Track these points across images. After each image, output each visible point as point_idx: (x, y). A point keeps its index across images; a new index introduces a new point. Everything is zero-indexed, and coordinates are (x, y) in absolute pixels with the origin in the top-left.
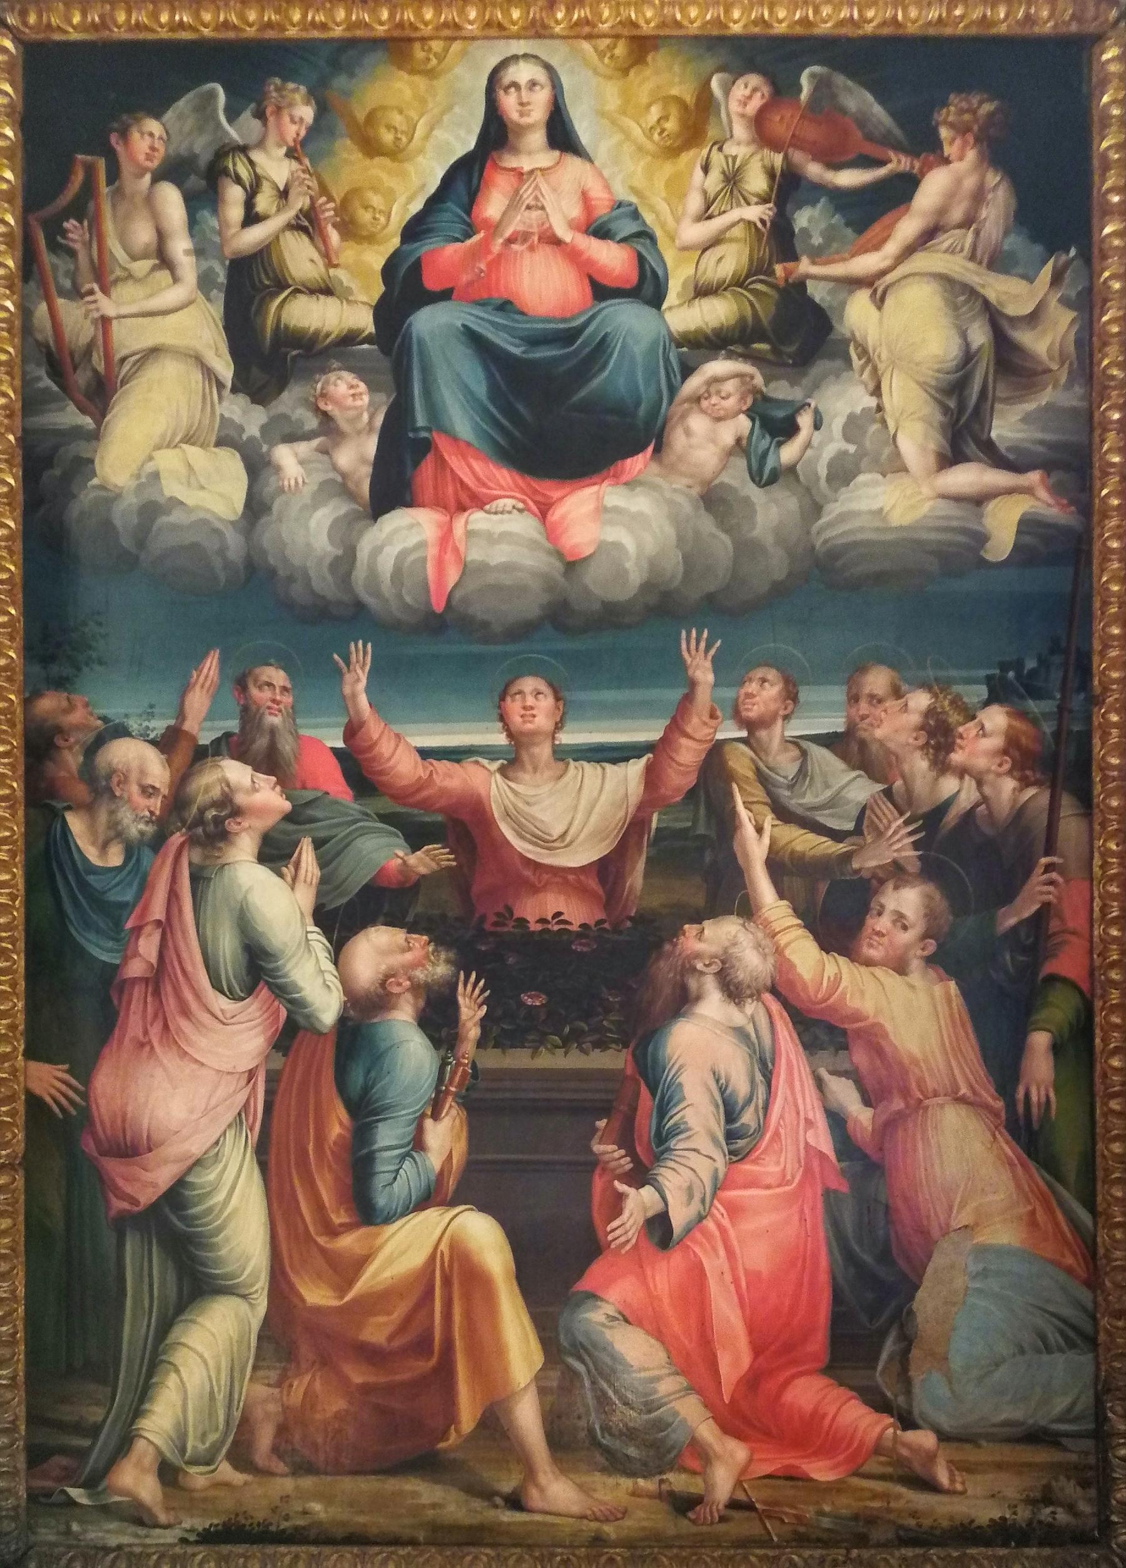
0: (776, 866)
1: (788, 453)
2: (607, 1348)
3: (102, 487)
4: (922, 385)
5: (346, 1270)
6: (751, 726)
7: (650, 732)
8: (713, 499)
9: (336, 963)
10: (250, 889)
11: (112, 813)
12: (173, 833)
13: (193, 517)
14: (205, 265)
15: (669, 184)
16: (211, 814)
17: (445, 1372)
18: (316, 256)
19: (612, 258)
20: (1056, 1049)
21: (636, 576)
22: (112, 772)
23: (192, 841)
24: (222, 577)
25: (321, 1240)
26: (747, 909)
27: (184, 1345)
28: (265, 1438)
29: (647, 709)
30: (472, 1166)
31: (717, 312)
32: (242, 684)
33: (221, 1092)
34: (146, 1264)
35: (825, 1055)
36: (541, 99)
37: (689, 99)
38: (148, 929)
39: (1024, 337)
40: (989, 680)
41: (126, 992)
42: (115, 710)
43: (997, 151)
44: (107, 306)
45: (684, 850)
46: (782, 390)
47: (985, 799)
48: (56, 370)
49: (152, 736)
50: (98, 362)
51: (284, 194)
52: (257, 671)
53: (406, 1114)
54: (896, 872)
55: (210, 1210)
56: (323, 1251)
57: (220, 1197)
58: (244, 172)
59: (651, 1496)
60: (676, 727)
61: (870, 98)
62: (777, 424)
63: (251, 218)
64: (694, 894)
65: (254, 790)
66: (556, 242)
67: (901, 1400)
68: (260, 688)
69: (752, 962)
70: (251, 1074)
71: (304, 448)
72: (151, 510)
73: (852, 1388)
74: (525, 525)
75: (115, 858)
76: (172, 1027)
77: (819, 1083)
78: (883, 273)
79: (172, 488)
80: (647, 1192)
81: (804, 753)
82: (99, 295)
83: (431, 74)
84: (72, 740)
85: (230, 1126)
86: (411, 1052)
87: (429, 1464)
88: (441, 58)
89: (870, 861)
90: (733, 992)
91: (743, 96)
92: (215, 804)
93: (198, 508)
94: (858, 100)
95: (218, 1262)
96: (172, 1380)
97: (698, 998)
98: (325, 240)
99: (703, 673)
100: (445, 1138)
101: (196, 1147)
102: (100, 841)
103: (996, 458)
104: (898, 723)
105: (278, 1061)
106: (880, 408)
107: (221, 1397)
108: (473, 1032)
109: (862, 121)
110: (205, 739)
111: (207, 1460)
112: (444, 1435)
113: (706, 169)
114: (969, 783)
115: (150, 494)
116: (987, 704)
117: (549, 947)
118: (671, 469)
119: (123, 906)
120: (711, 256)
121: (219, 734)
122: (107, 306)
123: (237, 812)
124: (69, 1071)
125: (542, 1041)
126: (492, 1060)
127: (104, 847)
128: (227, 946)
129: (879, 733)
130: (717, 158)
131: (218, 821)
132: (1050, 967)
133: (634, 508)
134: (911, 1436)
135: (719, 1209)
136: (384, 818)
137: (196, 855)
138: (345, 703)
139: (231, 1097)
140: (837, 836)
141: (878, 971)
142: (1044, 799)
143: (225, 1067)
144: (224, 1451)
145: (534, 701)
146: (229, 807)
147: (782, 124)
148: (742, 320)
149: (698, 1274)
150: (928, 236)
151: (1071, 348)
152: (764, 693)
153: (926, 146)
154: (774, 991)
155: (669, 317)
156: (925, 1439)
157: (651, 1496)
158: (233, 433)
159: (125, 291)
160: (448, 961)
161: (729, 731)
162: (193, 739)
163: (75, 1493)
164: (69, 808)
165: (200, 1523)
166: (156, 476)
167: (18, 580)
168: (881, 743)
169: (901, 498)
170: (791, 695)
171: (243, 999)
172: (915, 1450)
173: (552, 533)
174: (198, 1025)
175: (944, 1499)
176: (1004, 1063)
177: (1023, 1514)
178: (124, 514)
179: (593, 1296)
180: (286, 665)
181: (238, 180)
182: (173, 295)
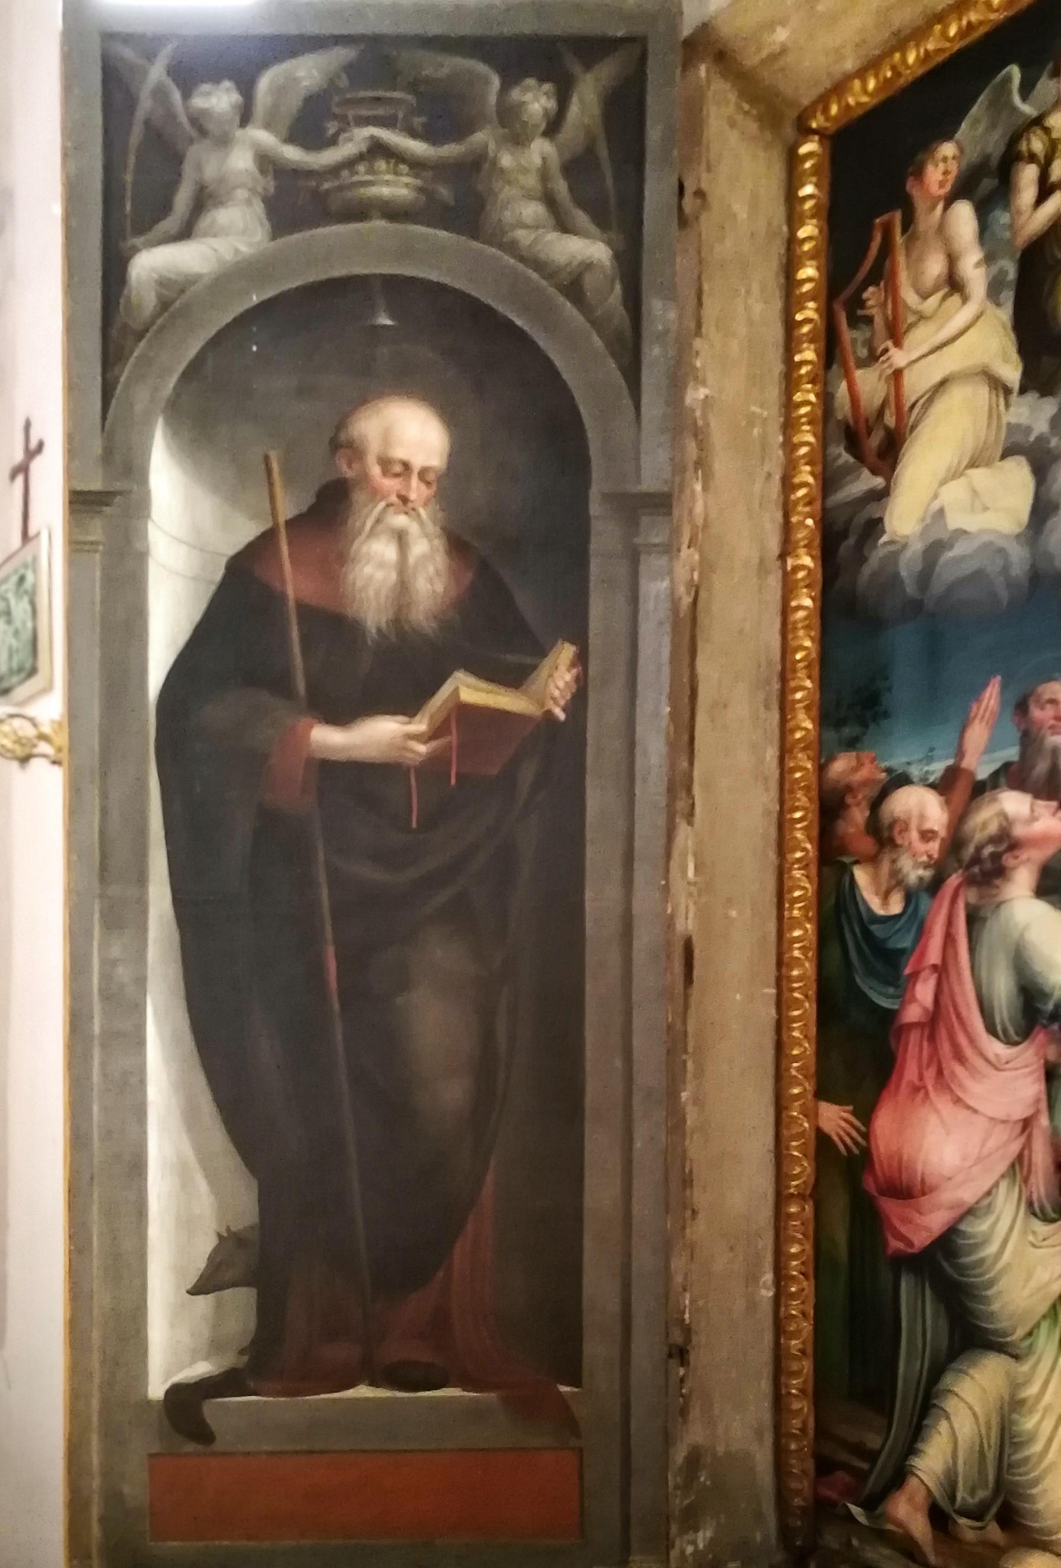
10: (1027, 927)
11: (894, 861)
12: (950, 875)
13: (976, 544)
14: (995, 269)
22: (894, 822)
23: (970, 881)
24: (1004, 595)
27: (957, 1395)
32: (1022, 707)
33: (992, 1143)
34: (920, 1302)
41: (903, 1037)
42: (897, 762)
44: (899, 358)
49: (932, 779)
50: (890, 420)
52: (1041, 689)
55: (982, 1261)
57: (992, 1249)
65: (1033, 818)
68: (1042, 708)
70: (1027, 1124)
72: (934, 550)
75: (896, 906)
76: (946, 1072)
79: (955, 521)
82: (893, 351)
84: (860, 797)
85: (1003, 1176)
92: (993, 840)
93: (982, 531)
95: (991, 1316)
96: (943, 1426)
101: (968, 1195)
102: (884, 888)
107: (991, 1455)
110: (983, 773)
111: (977, 1514)
115: (935, 535)
119: (902, 952)
121: (996, 766)
124: (854, 1113)
127: (886, 897)
128: (1003, 988)
131: (996, 857)
137: (971, 895)
143: (1000, 1114)
144: (994, 1510)
146: (1007, 842)
158: (1019, 438)
162: (971, 774)
163: (855, 1510)
164: (857, 862)
167: (814, 655)
171: (1016, 1044)
174: (973, 1072)
178: (908, 567)
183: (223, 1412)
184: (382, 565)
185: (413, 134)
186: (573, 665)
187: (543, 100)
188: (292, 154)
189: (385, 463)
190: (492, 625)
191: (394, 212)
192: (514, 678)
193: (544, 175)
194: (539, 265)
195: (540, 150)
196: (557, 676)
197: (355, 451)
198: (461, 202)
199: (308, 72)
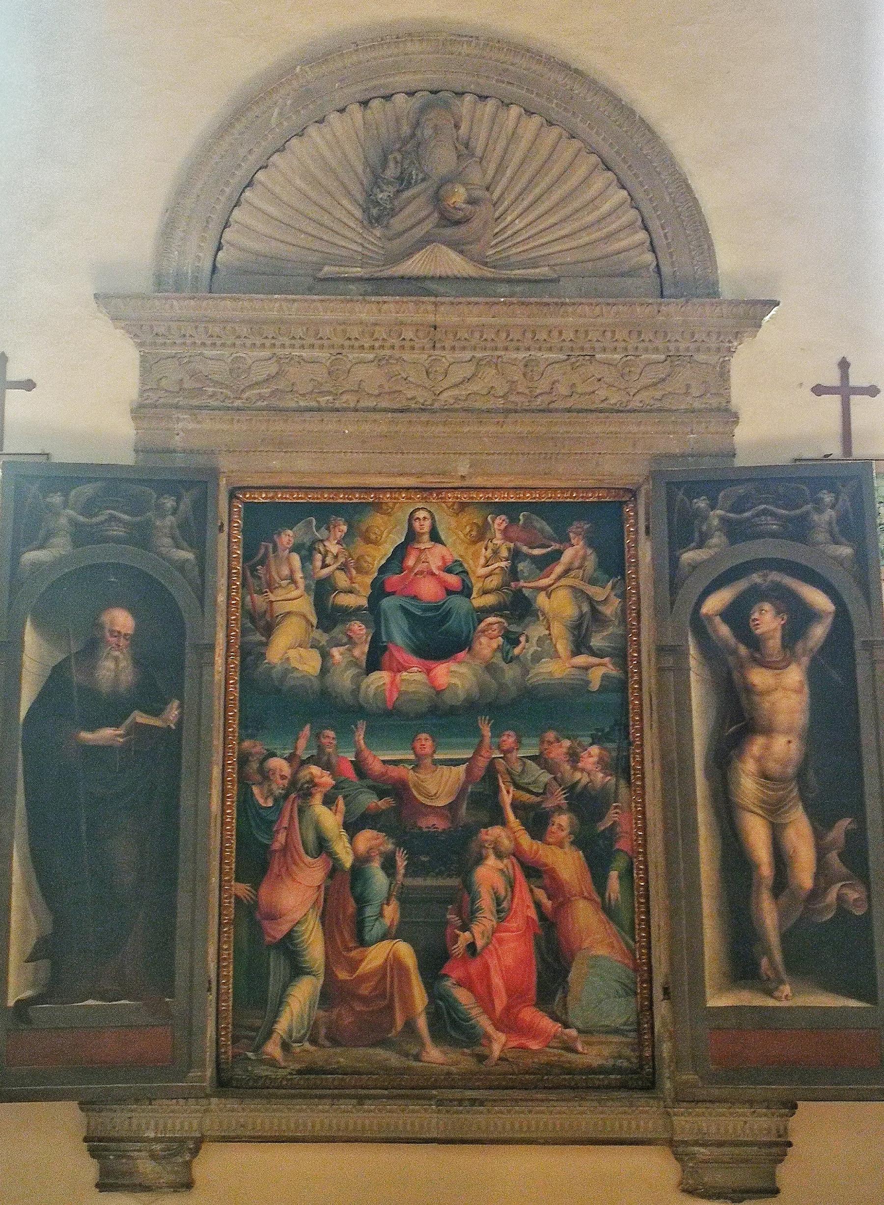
0: (515, 806)
1: (517, 651)
2: (450, 996)
3: (269, 663)
4: (566, 626)
5: (353, 965)
6: (505, 752)
7: (467, 754)
8: (490, 668)
9: (351, 844)
11: (269, 785)
15: (473, 554)
16: (306, 786)
17: (390, 1007)
18: (347, 579)
19: (453, 580)
20: (620, 877)
21: (462, 695)
23: (299, 796)
25: (344, 953)
26: (504, 823)
28: (323, 1031)
29: (465, 746)
30: (402, 923)
31: (490, 600)
32: (318, 736)
33: (307, 895)
35: (533, 880)
36: (427, 524)
37: (480, 524)
38: (282, 831)
39: (601, 608)
40: (592, 736)
43: (590, 543)
45: (483, 797)
46: (514, 628)
47: (591, 781)
48: (253, 620)
51: (336, 557)
53: (376, 903)
54: (559, 809)
55: (303, 941)
56: (344, 956)
58: (322, 549)
59: (469, 1055)
60: (477, 752)
61: (544, 523)
62: (512, 640)
63: (324, 566)
64: (484, 816)
66: (433, 574)
67: (564, 1017)
69: (506, 844)
71: (342, 649)
73: (546, 1012)
74: (421, 677)
77: (531, 891)
78: (550, 585)
79: (294, 664)
80: (467, 934)
81: (524, 763)
83: (389, 515)
86: (379, 879)
87: (383, 1043)
88: (392, 509)
89: (549, 804)
90: (499, 856)
91: (499, 523)
92: (308, 782)
94: (540, 524)
97: (486, 858)
98: (351, 574)
99: (487, 731)
100: (391, 912)
101: (298, 916)
103: (594, 654)
104: (559, 750)
105: (330, 882)
106: (550, 634)
108: (402, 871)
109: (542, 531)
110: (305, 757)
111: (300, 1041)
112: (389, 1031)
113: (486, 549)
114: (585, 774)
115: (286, 666)
116: (591, 744)
117: (431, 837)
118: (474, 657)
119: (272, 822)
120: (490, 579)
122: (272, 597)
123: (316, 785)
125: (427, 874)
126: (409, 882)
128: (311, 837)
129: (552, 755)
130: (490, 544)
132: (617, 847)
133: (461, 671)
134: (567, 1030)
135: (494, 941)
136: (369, 787)
138: (356, 743)
139: (311, 896)
140: (537, 795)
141: (553, 847)
142: (614, 781)
145: (425, 741)
146: (313, 783)
147: (514, 532)
148: (500, 603)
149: (487, 968)
150: (566, 572)
151: (619, 611)
152: (509, 739)
153: (565, 540)
154: (514, 855)
155: (473, 601)
156: (573, 1032)
157: (469, 1055)
159: (279, 591)
160: (393, 843)
161: (497, 754)
163: (250, 1054)
165: (297, 1066)
166: (288, 659)
168: (552, 759)
169: (557, 667)
170: (519, 741)
172: (569, 1037)
173: (432, 681)
175: (579, 1056)
176: (600, 882)
177: (611, 1062)
179: (445, 975)
180: (333, 728)
181: (320, 553)
182: (295, 593)
183: (35, 1011)
184: (109, 670)
185: (125, 513)
186: (178, 708)
187: (171, 502)
188: (81, 519)
189: (112, 632)
190: (150, 693)
191: (117, 540)
192: (156, 713)
193: (172, 528)
194: (170, 561)
195: (170, 520)
196: (173, 712)
197: (101, 627)
198: (142, 537)
199: (88, 490)
